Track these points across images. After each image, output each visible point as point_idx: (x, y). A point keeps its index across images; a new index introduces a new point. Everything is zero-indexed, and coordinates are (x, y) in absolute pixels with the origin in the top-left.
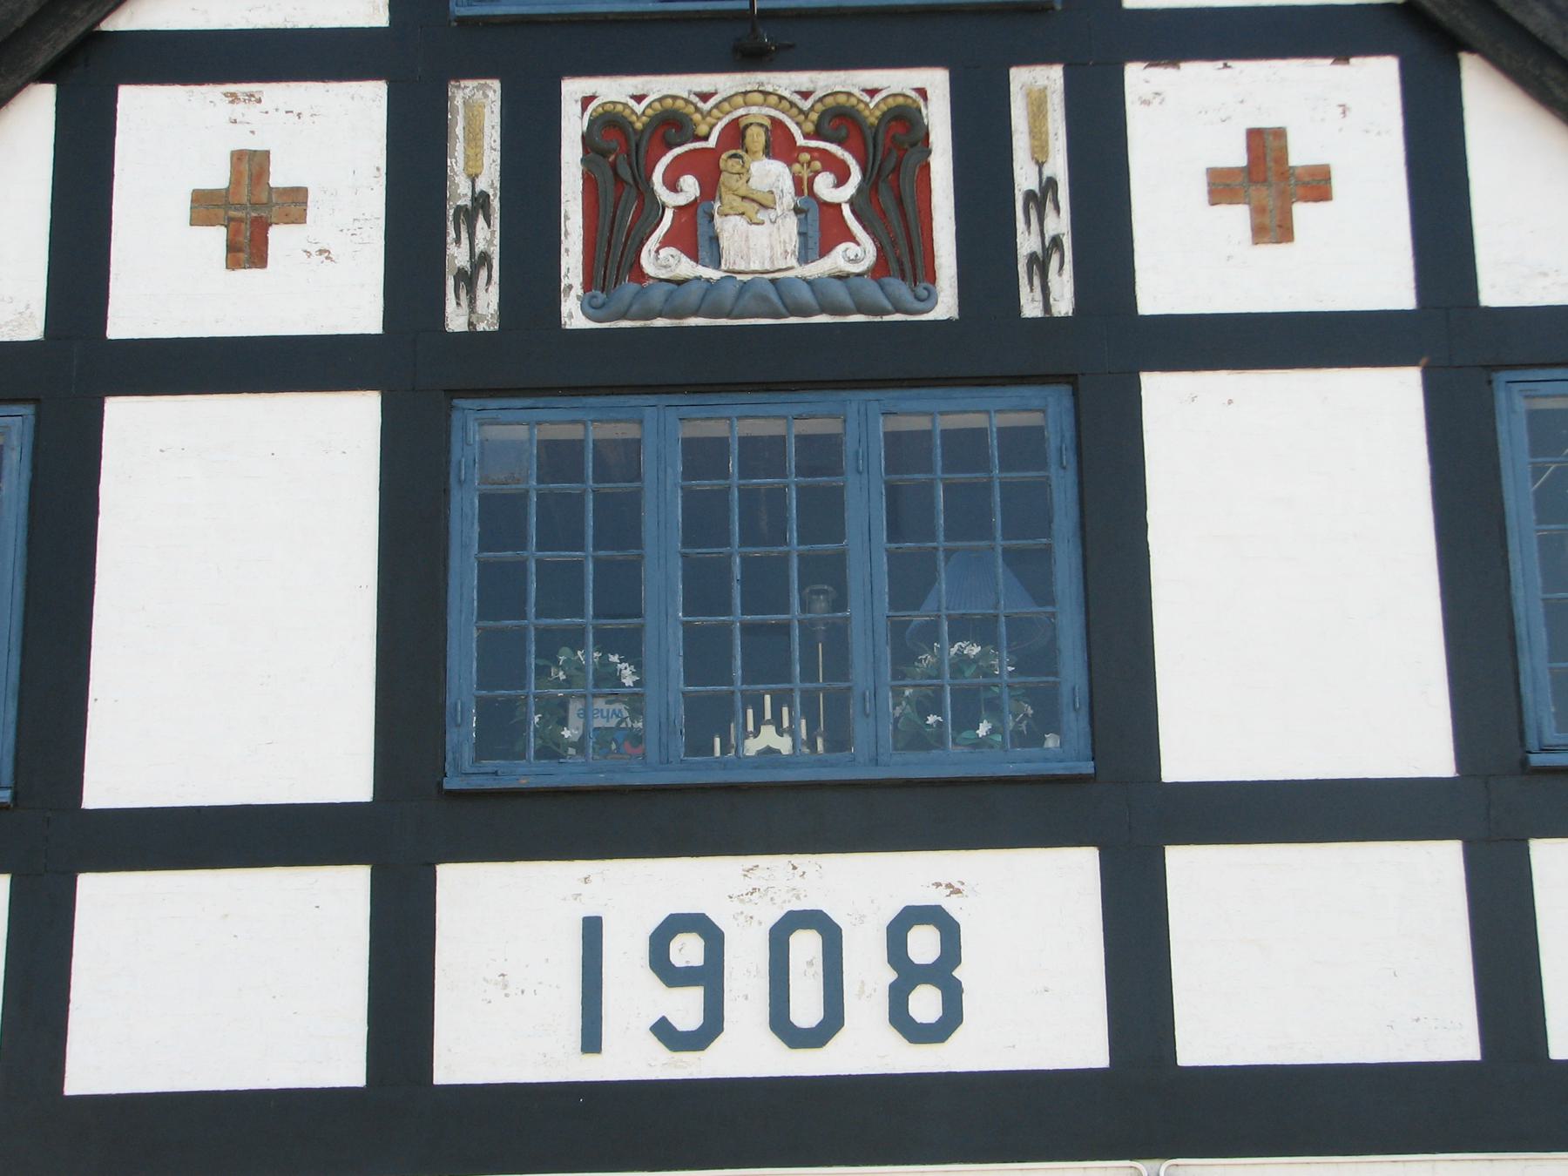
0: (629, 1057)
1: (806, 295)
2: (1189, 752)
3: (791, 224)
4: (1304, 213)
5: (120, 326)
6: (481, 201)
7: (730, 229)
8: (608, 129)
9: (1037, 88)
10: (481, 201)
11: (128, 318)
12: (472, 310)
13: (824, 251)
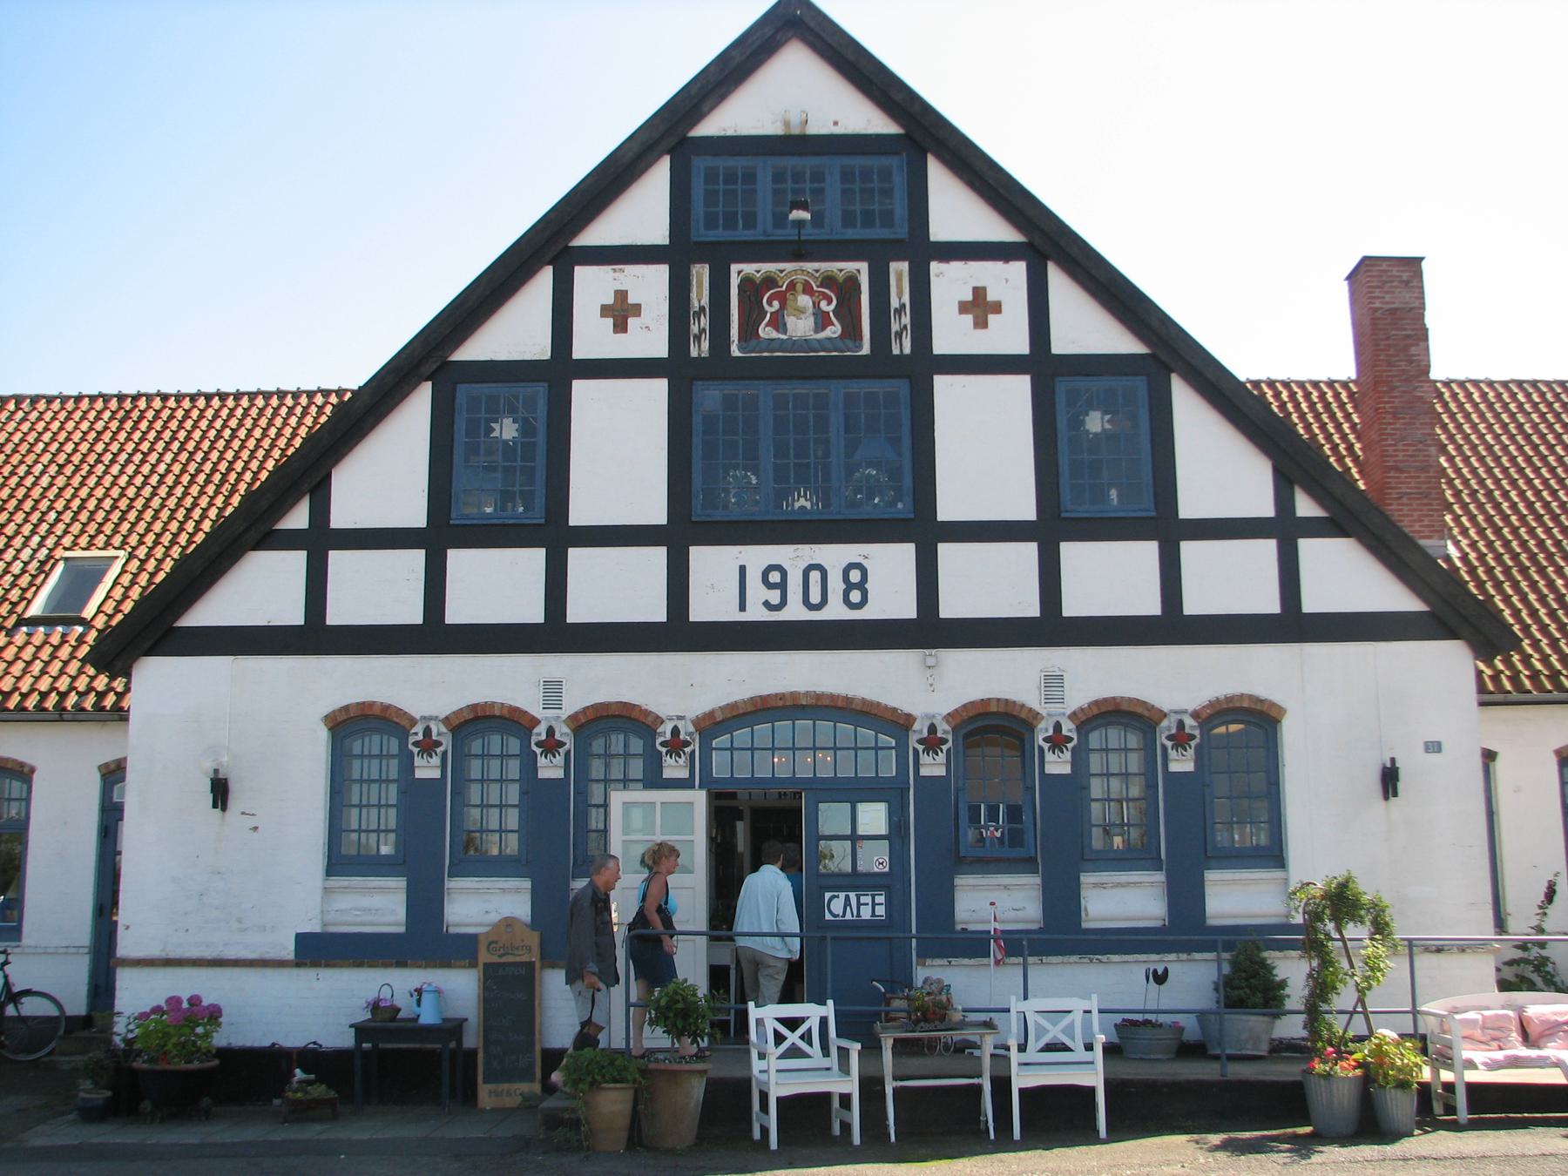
0: (755, 613)
1: (817, 345)
2: (949, 509)
3: (812, 319)
4: (991, 318)
5: (578, 353)
6: (702, 309)
7: (790, 321)
8: (746, 282)
9: (899, 269)
10: (702, 309)
11: (580, 351)
12: (700, 349)
13: (823, 329)
